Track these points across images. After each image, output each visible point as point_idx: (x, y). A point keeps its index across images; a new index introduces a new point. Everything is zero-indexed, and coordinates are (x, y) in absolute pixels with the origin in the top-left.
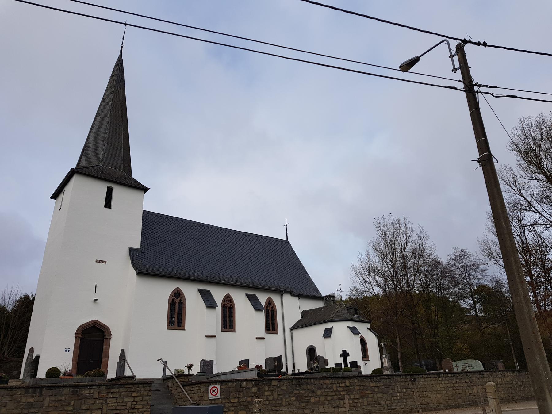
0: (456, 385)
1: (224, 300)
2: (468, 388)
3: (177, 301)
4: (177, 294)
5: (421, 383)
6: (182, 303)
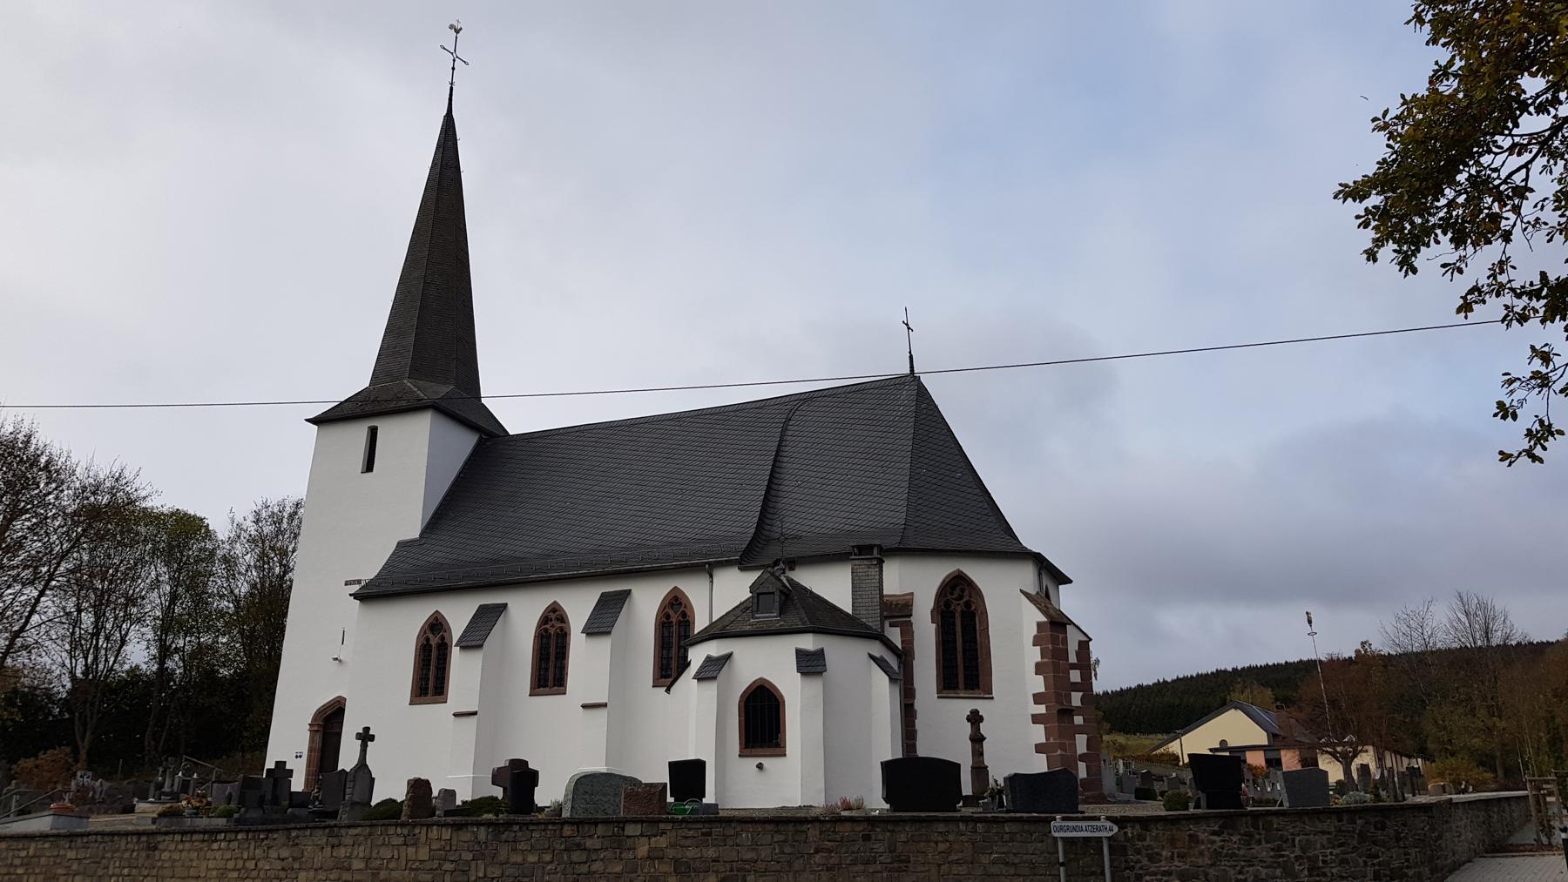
0: (251, 865)
1: (545, 620)
2: (282, 874)
3: (434, 641)
4: (436, 625)
5: (166, 855)
6: (973, 614)
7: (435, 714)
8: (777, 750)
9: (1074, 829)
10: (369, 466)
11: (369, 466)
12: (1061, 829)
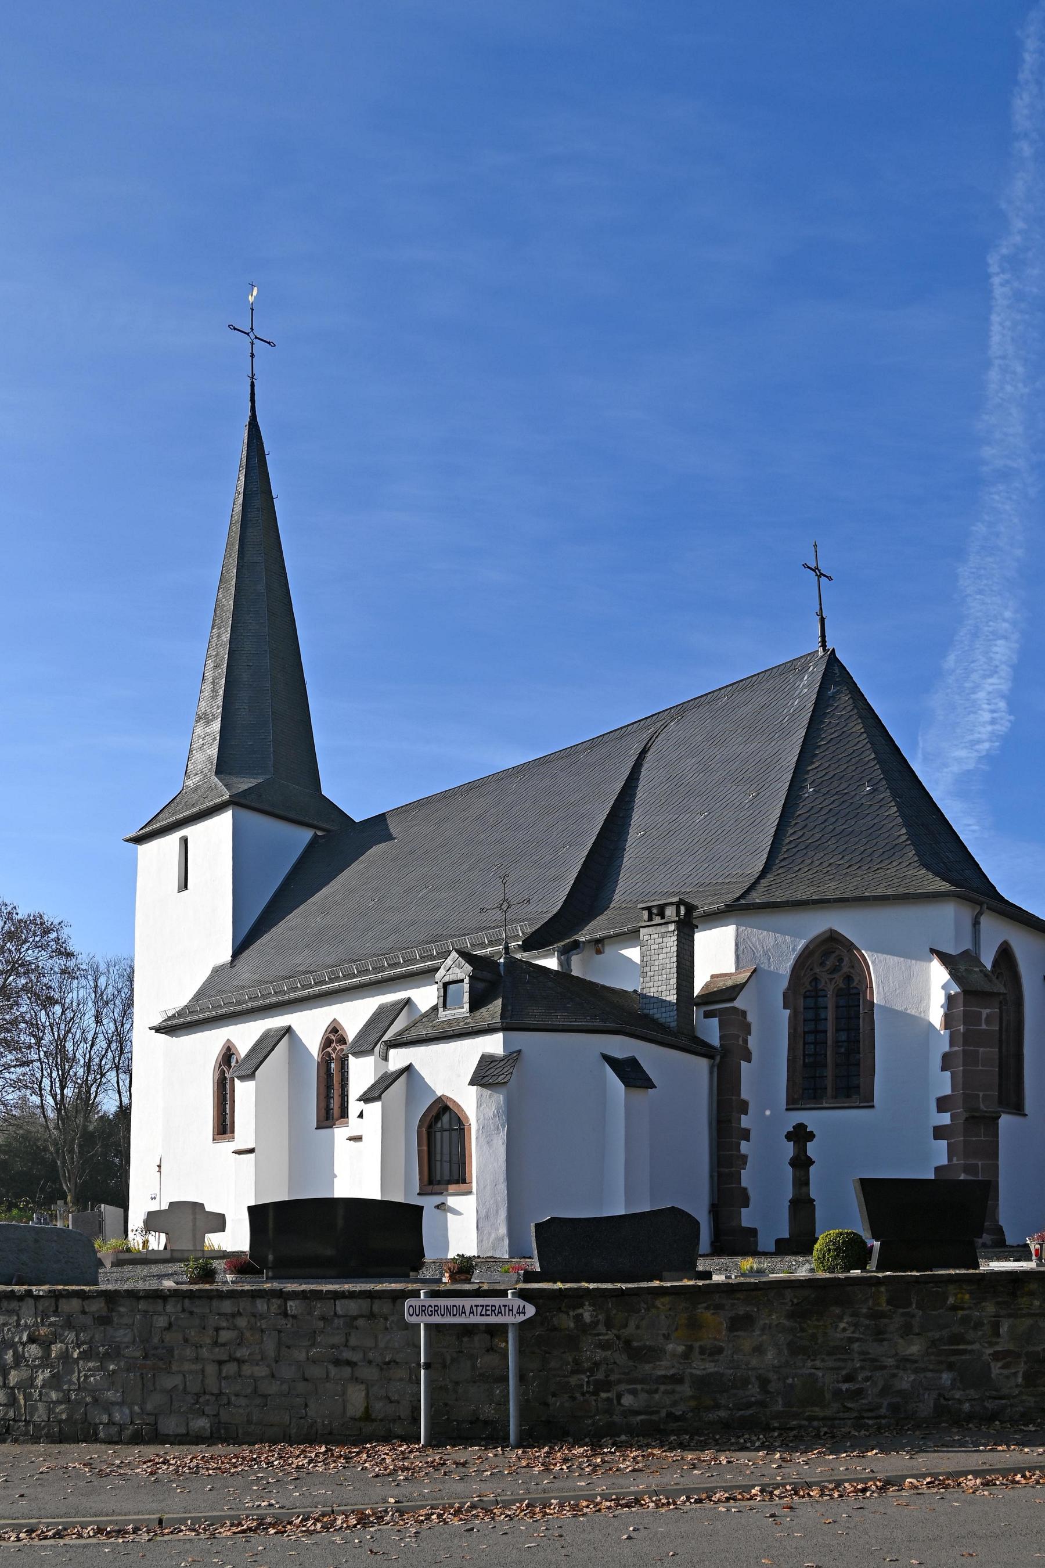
7: (227, 1147)
8: (463, 1186)
9: (448, 1310)
10: (184, 885)
11: (184, 885)
12: (423, 1310)
